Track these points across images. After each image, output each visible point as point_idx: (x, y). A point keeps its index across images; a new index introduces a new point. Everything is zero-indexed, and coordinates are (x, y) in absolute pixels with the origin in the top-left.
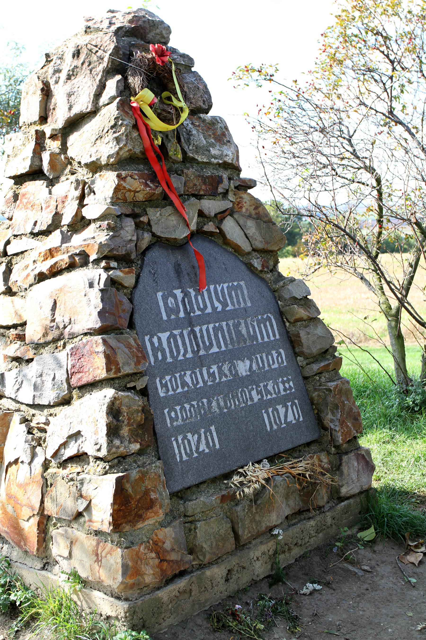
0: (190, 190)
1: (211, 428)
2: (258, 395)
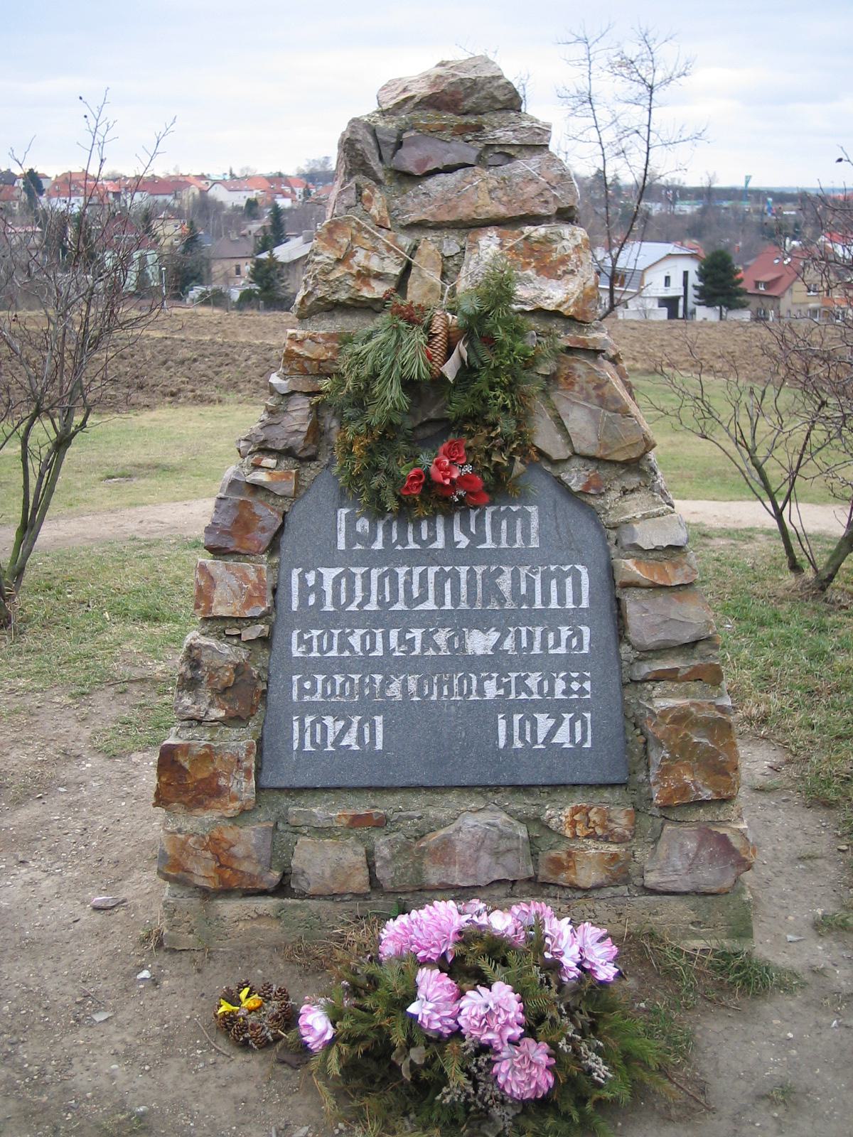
1: (376, 718)
2: (498, 689)
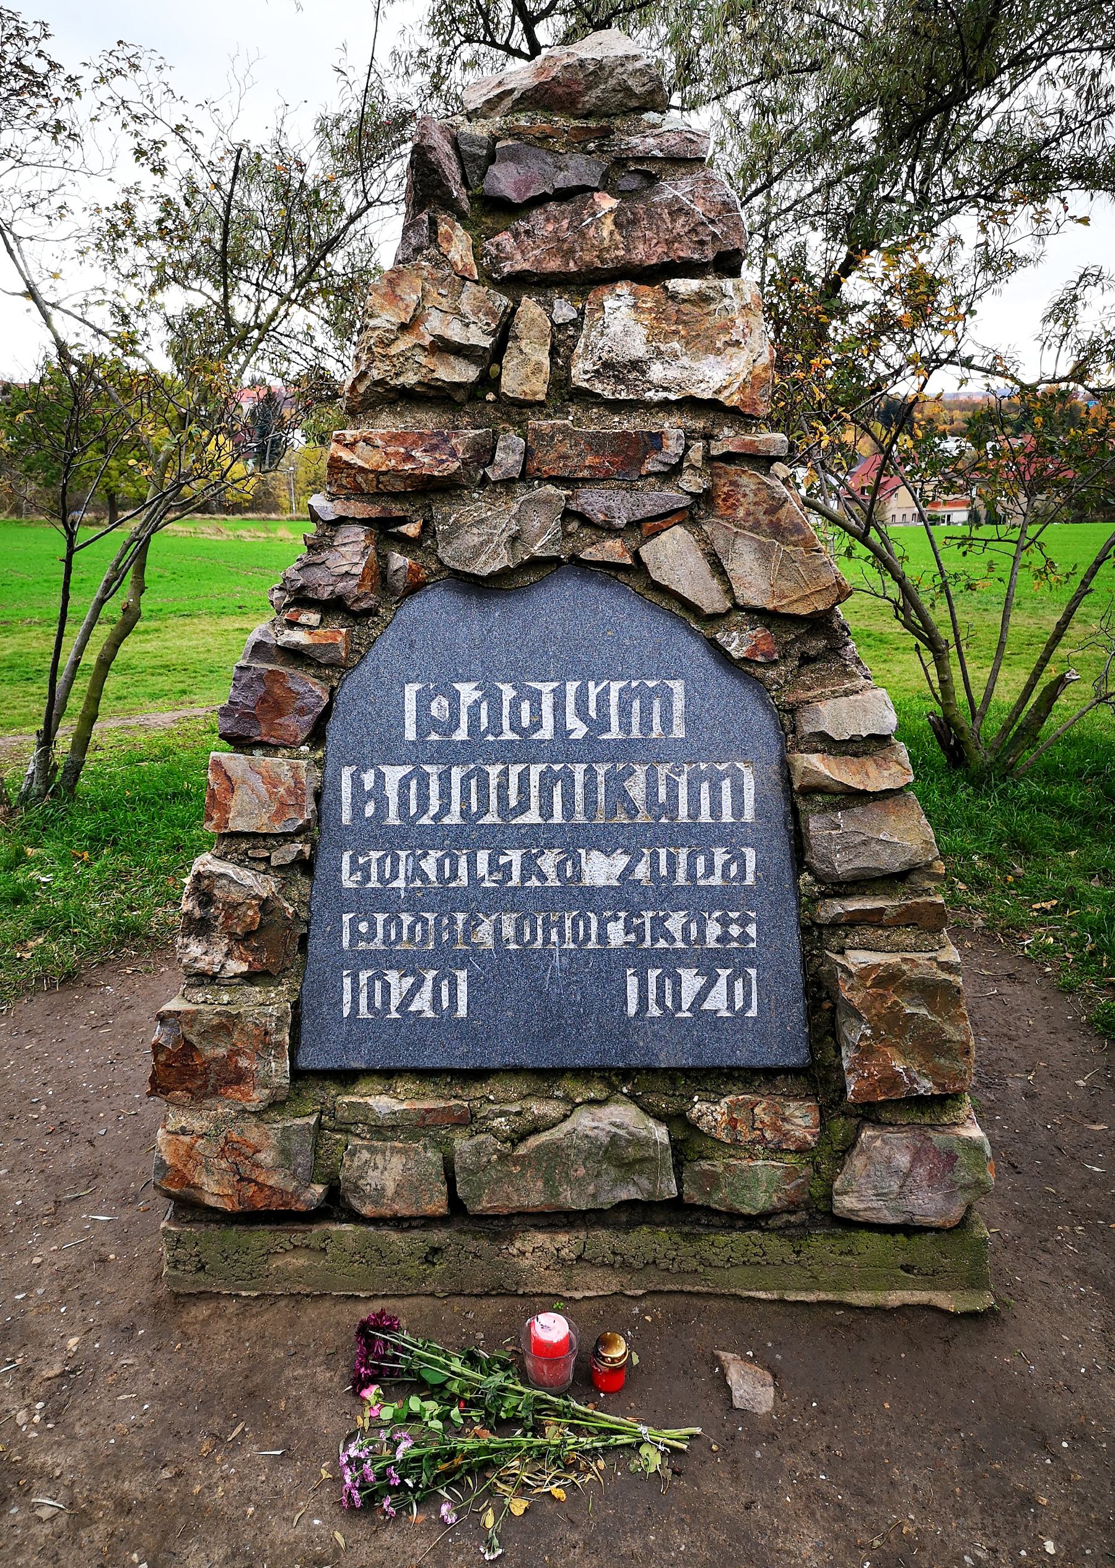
0: (546, 468)
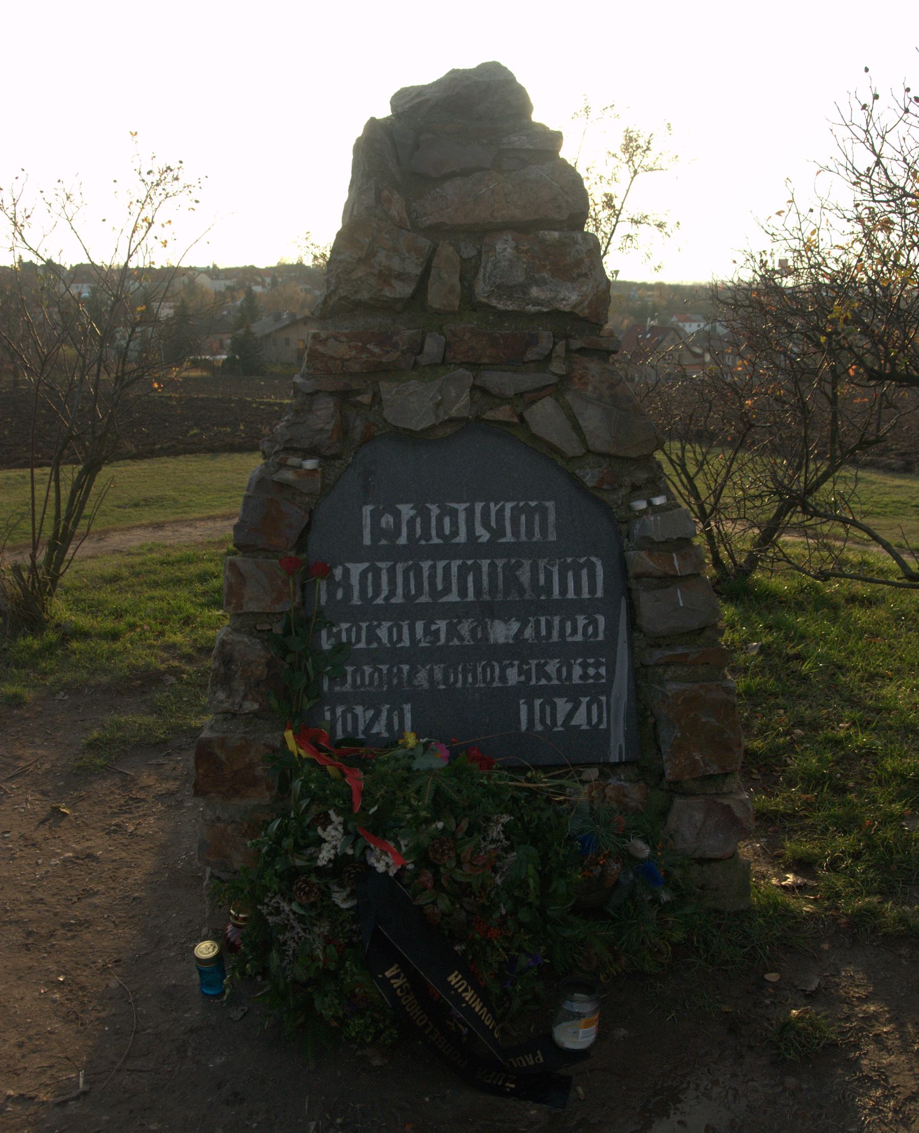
1: (404, 706)
